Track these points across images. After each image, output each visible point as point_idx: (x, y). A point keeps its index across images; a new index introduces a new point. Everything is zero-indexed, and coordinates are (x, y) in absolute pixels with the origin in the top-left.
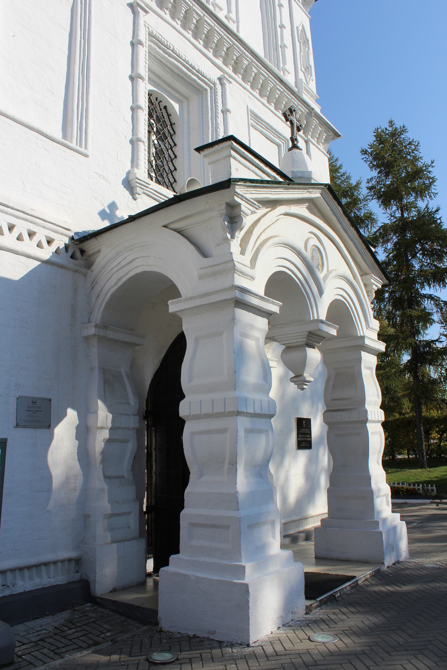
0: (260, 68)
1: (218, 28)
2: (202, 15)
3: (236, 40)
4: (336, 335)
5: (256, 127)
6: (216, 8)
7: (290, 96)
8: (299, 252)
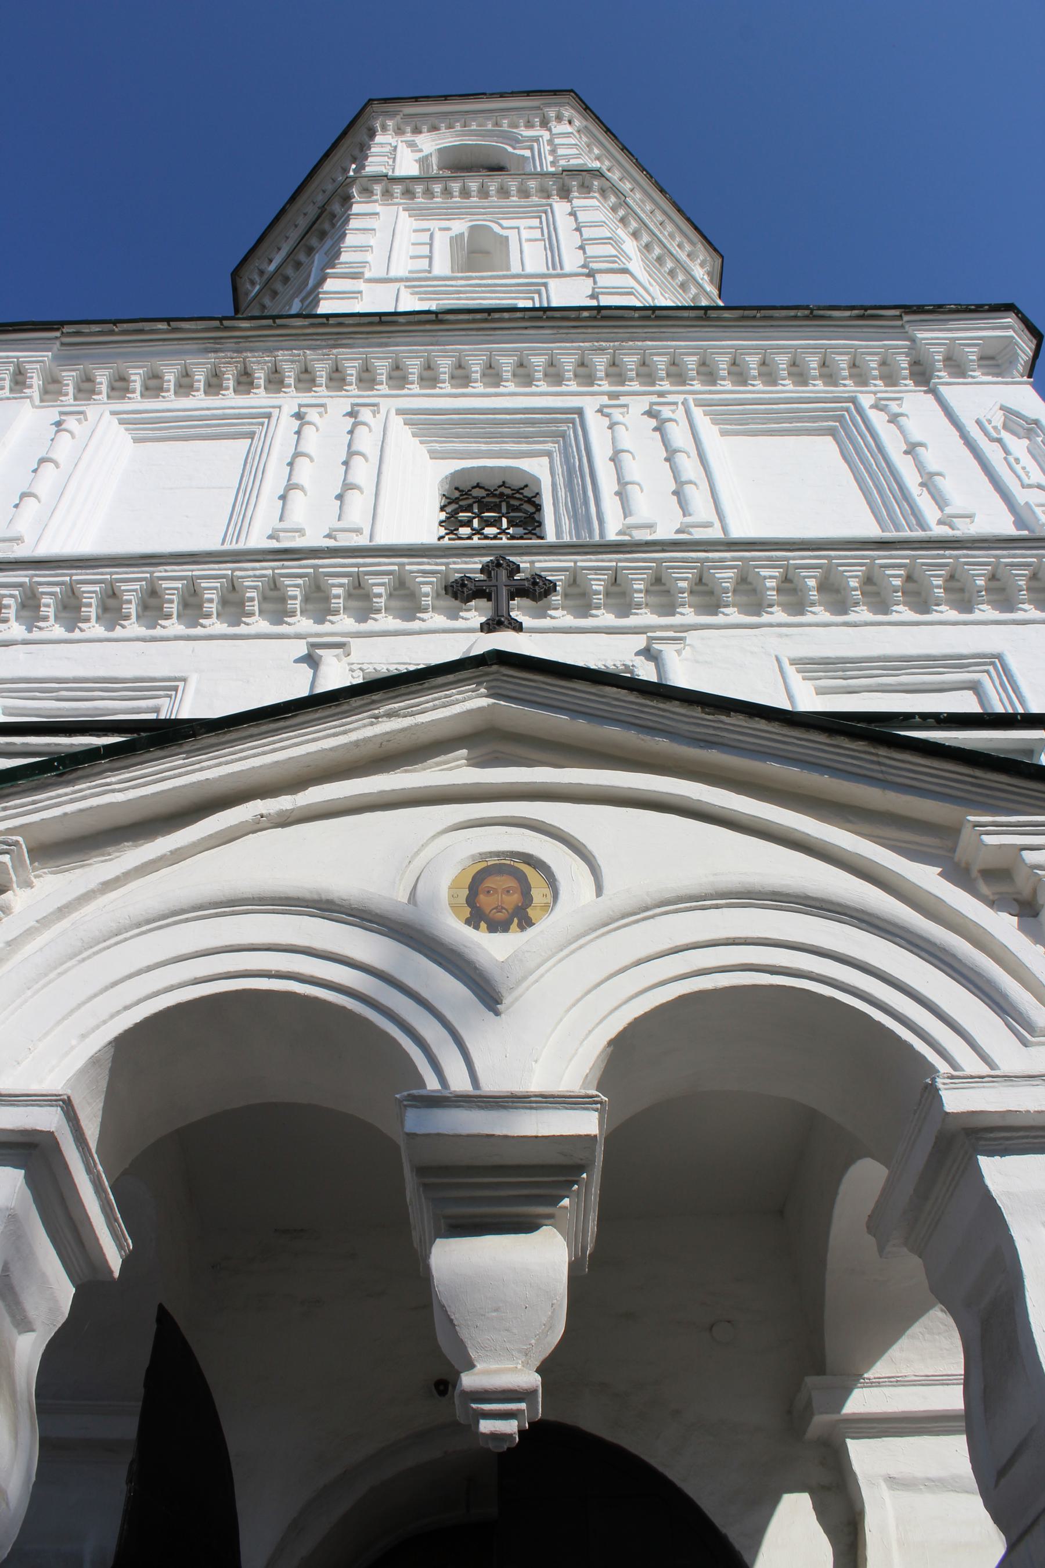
0: (787, 559)
1: (591, 561)
2: (572, 564)
3: (663, 551)
4: (983, 1161)
5: (849, 686)
6: (692, 530)
7: (944, 557)
8: (320, 901)
